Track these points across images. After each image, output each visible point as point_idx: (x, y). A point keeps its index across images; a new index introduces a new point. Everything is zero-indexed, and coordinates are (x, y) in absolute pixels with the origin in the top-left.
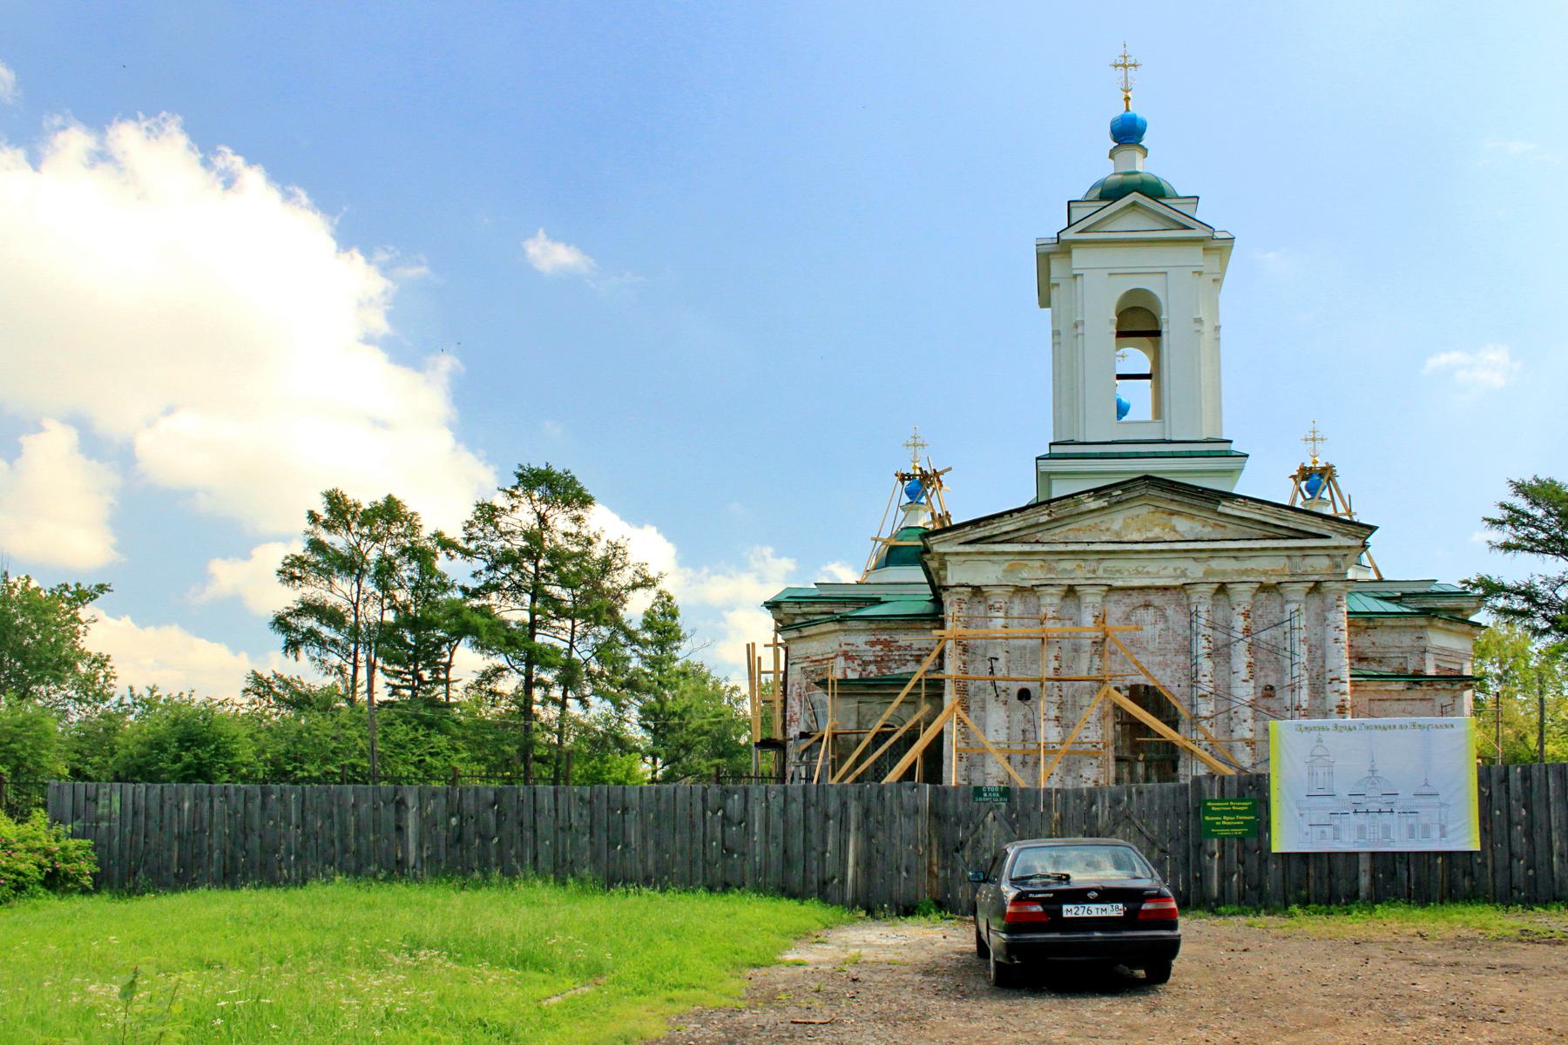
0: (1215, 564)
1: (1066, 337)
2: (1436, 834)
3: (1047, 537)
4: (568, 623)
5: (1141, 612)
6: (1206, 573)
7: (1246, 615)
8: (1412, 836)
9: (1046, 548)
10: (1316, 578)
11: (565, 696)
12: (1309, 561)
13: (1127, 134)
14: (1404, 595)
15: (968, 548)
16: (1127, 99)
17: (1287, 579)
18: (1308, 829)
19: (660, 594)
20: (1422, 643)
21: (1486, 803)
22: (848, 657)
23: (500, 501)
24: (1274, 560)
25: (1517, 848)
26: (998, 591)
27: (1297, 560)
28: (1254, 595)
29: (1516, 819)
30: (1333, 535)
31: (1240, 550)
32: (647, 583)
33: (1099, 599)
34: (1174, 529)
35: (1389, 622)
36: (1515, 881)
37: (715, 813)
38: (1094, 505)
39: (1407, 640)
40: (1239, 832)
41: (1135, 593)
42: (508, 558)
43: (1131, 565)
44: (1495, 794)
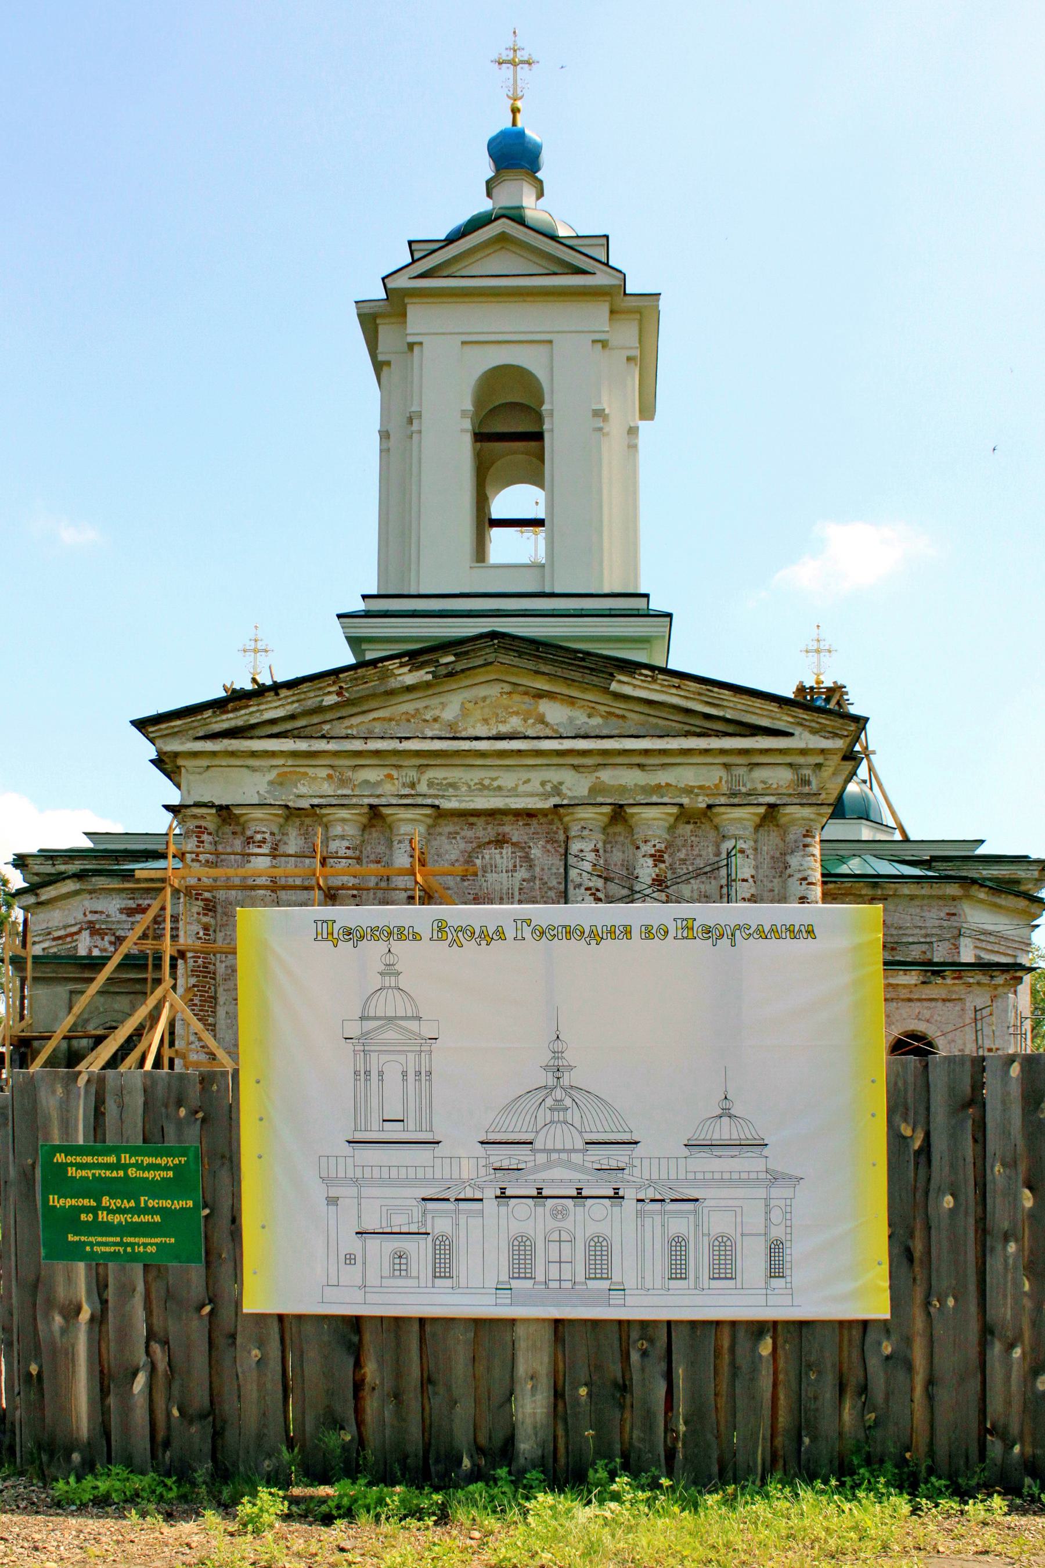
0: (606, 776)
1: (400, 434)
2: (752, 1262)
3: (340, 729)
5: (491, 853)
6: (593, 790)
7: (658, 858)
8: (678, 1271)
9: (332, 746)
10: (771, 800)
12: (759, 774)
13: (514, 156)
14: (934, 859)
15: (209, 746)
16: (515, 111)
17: (723, 800)
18: (355, 1245)
20: (954, 922)
21: (911, 1170)
22: (94, 930)
24: (704, 770)
25: (1003, 1310)
26: (258, 813)
27: (741, 771)
28: (672, 828)
29: (1000, 1218)
30: (797, 730)
31: (646, 752)
33: (422, 829)
34: (542, 720)
35: (906, 890)
36: (996, 1406)
38: (410, 678)
39: (933, 916)
40: (148, 1245)
41: (480, 822)
43: (474, 776)
44: (940, 1145)
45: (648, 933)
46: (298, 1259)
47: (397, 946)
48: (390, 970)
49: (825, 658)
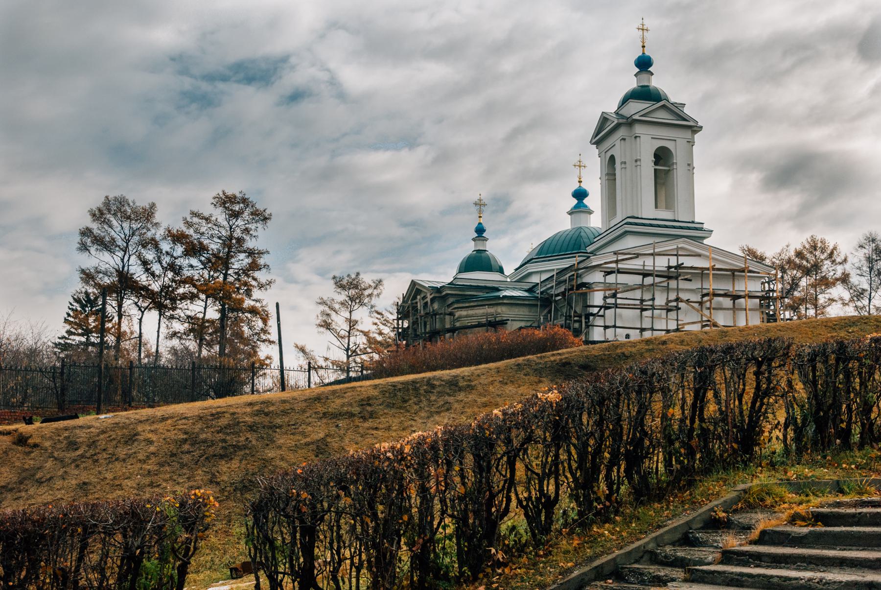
13: (644, 64)
16: (643, 47)
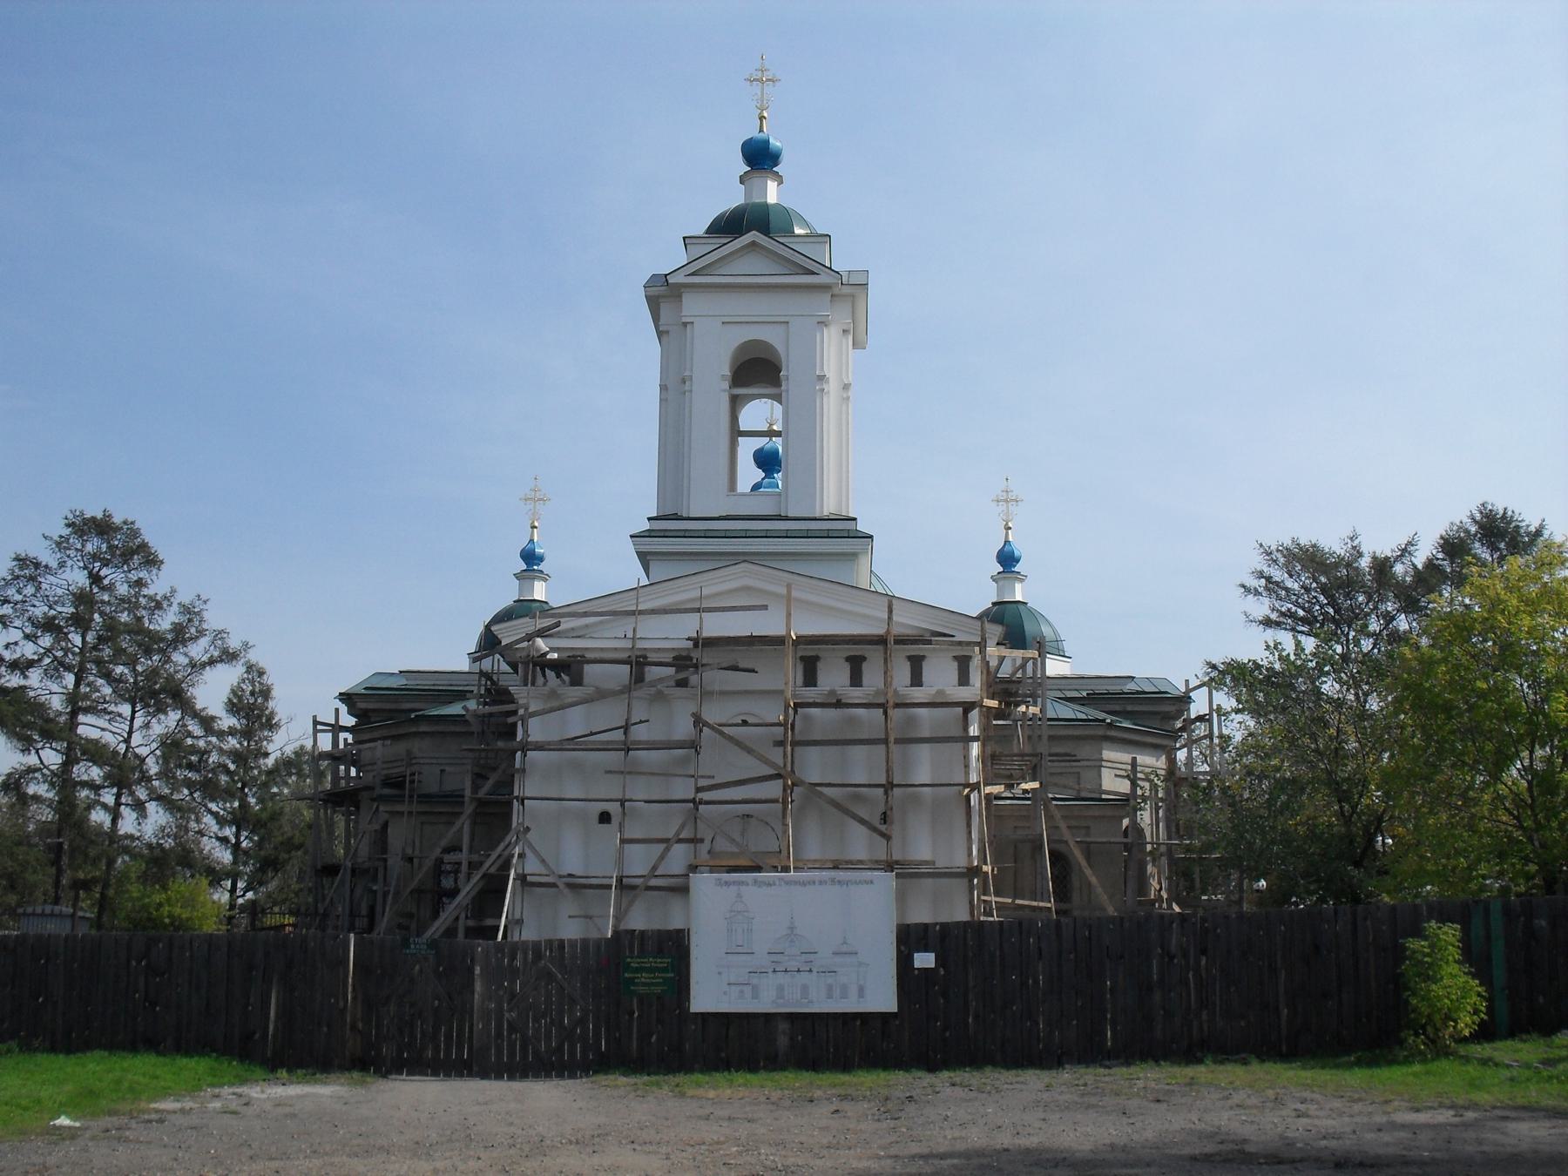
1: (675, 388)
2: (854, 991)
4: (126, 709)
8: (830, 996)
11: (118, 804)
19: (250, 668)
23: (48, 557)
32: (229, 656)
37: (139, 962)
40: (658, 990)
42: (49, 625)
45: (821, 883)
46: (712, 991)
47: (743, 888)
48: (739, 896)
49: (1012, 508)
